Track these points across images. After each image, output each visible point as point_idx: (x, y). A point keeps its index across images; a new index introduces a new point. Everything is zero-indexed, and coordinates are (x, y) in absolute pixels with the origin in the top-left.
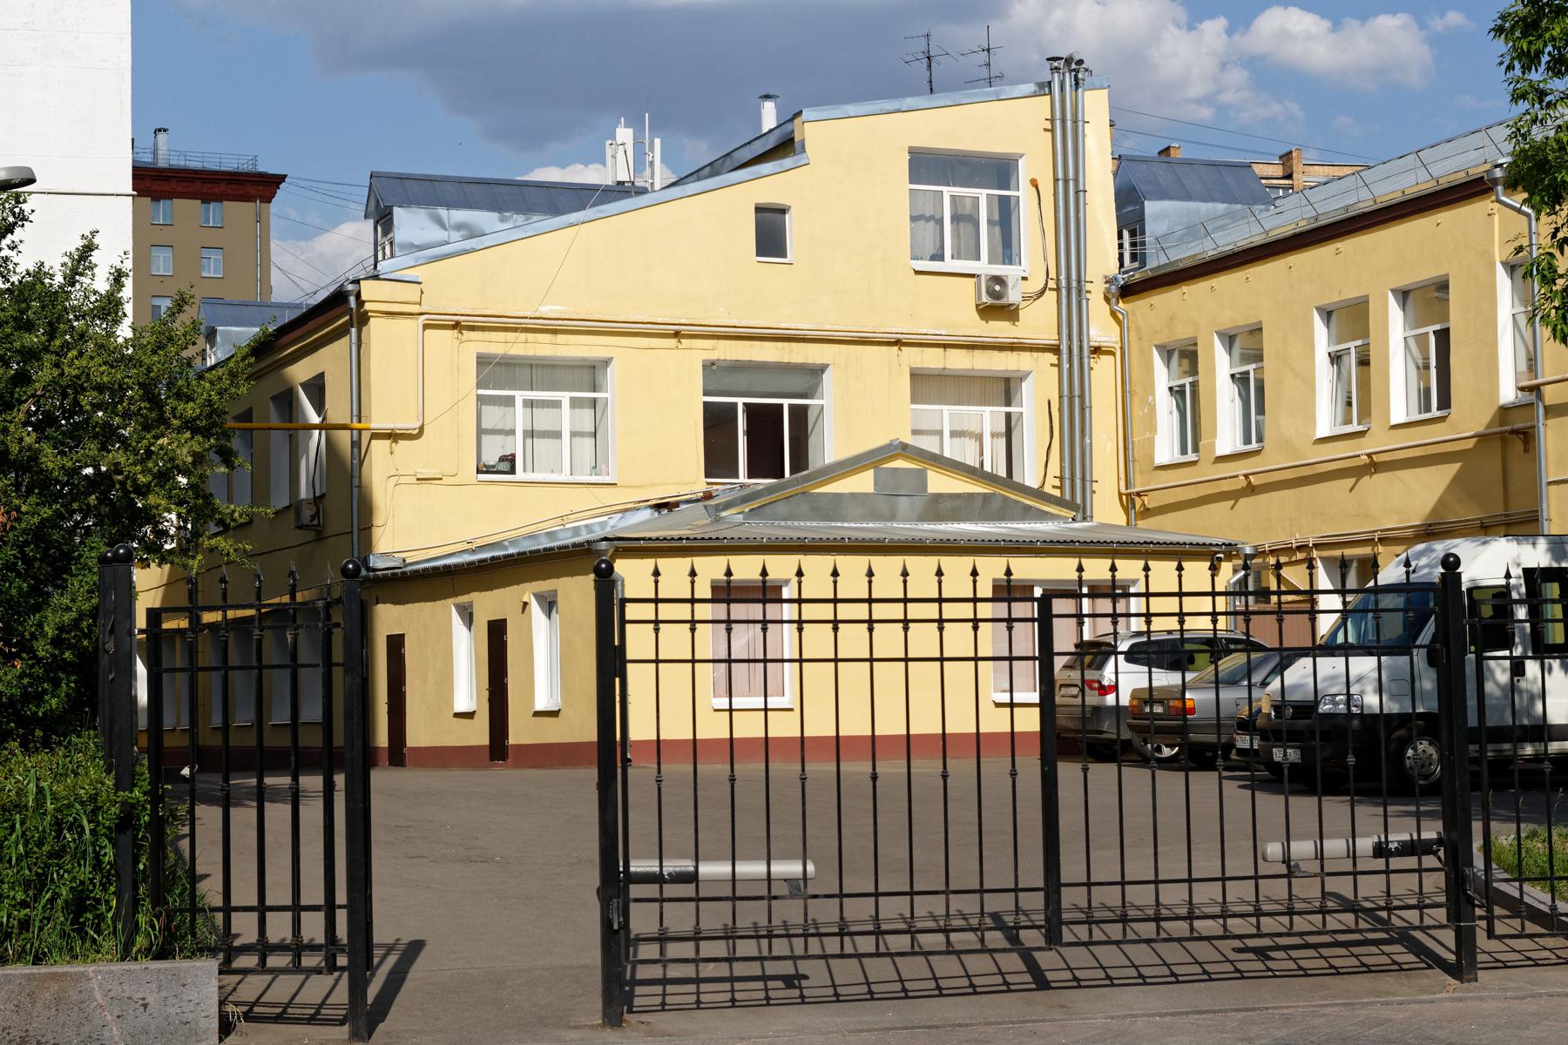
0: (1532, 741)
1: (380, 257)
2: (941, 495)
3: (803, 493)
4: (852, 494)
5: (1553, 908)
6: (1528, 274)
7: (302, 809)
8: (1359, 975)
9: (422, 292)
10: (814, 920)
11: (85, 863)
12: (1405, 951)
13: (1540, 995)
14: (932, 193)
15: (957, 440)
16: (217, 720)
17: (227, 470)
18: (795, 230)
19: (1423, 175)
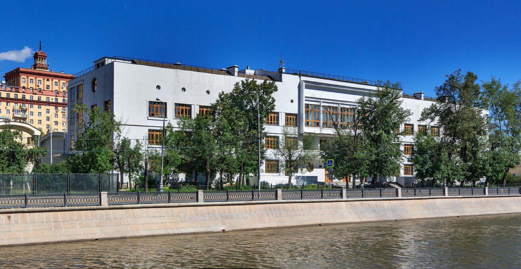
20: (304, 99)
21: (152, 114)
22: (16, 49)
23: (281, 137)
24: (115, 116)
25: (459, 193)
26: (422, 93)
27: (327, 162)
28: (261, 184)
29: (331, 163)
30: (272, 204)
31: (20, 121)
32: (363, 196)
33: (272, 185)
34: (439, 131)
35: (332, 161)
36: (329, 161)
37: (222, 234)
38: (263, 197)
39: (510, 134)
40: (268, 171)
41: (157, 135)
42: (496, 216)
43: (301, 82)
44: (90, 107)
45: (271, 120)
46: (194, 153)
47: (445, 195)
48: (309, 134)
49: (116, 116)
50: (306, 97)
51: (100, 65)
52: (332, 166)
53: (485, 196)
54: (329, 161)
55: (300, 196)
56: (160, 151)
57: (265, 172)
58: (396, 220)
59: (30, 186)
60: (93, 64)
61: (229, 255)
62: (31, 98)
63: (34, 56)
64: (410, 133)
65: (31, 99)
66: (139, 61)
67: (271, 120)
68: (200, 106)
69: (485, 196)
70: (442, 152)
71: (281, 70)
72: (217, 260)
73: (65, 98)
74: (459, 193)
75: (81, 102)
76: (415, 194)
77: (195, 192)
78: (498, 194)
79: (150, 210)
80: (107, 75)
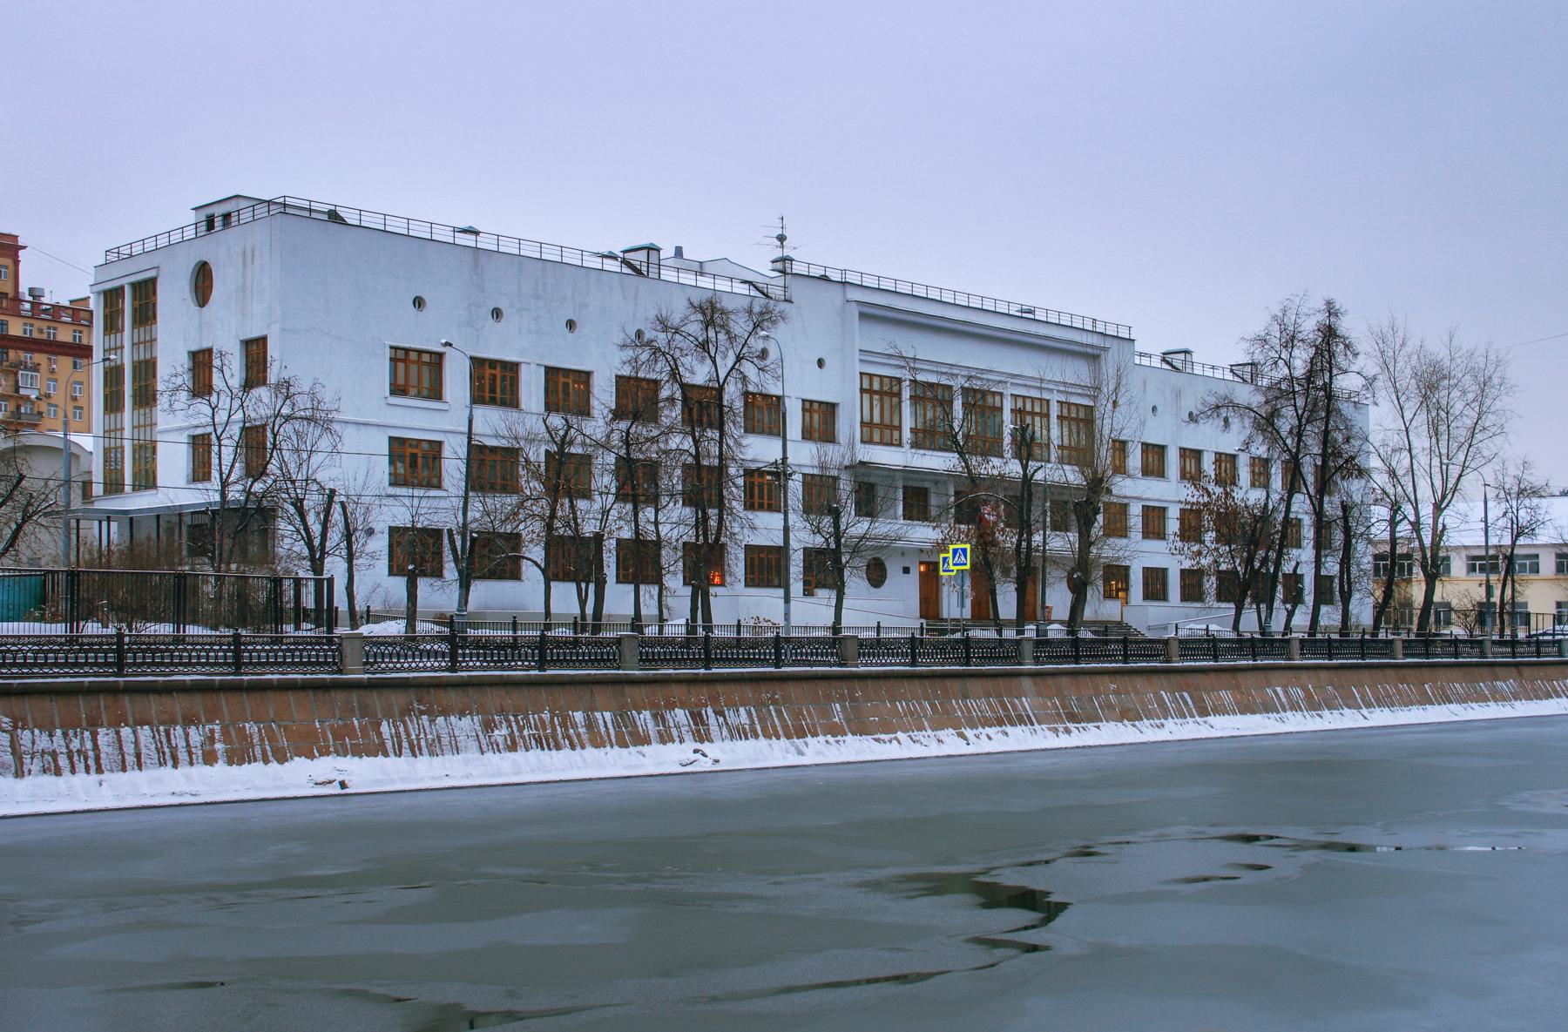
0: (1253, 561)
1: (1031, 316)
2: (546, 404)
3: (1440, 848)
4: (1253, 712)
5: (67, 442)
6: (401, 458)
7: (1483, 516)
8: (417, 411)
9: (781, 238)
10: (31, 291)
11: (978, 378)
12: (632, 273)
13: (957, 375)
14: (130, 576)
15: (128, 521)
16: (1509, 597)
17: (73, 438)
18: (1399, 846)
19: (1549, 672)
21: (398, 390)
23: (738, 506)
24: (16, 237)
27: (950, 555)
29: (963, 558)
35: (964, 550)
36: (955, 551)
39: (237, 495)
40: (753, 580)
44: (186, 356)
45: (761, 497)
48: (1066, 423)
51: (218, 223)
52: (965, 564)
54: (955, 551)
56: (1071, 478)
57: (743, 582)
60: (192, 218)
62: (75, 336)
65: (25, 333)
66: (358, 217)
67: (761, 497)
68: (546, 367)
75: (148, 338)
80: (253, 256)
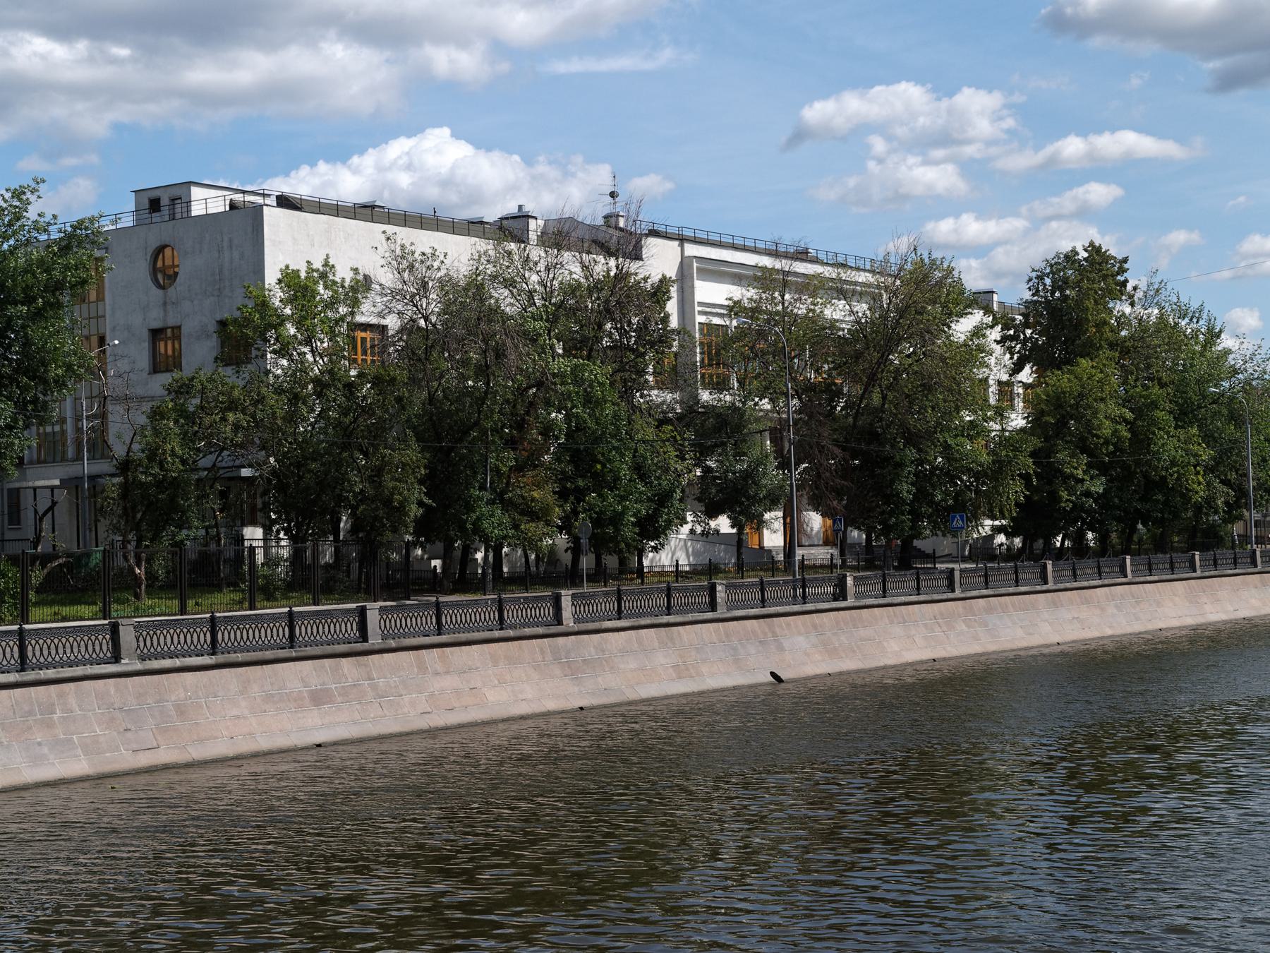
20: (698, 308)
22: (1095, 134)
25: (918, 589)
26: (993, 292)
28: (701, 330)
30: (841, 612)
31: (1079, 538)
32: (763, 603)
33: (680, 563)
34: (218, 534)
37: (578, 714)
38: (65, 652)
41: (364, 340)
42: (444, 740)
43: (686, 261)
46: (99, 446)
47: (1195, 571)
49: (1072, 245)
50: (700, 304)
53: (1045, 587)
55: (16, 655)
58: (581, 708)
59: (830, 89)
61: (439, 761)
63: (339, 166)
64: (1104, 548)
69: (1194, 575)
70: (1026, 325)
71: (520, 223)
72: (248, 839)
73: (1187, 320)
74: (918, 589)
75: (93, 314)
76: (763, 601)
77: (660, 590)
78: (885, 598)
79: (327, 665)
